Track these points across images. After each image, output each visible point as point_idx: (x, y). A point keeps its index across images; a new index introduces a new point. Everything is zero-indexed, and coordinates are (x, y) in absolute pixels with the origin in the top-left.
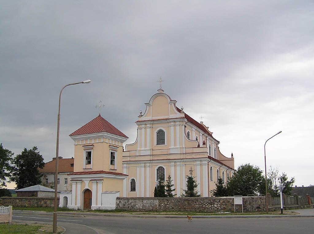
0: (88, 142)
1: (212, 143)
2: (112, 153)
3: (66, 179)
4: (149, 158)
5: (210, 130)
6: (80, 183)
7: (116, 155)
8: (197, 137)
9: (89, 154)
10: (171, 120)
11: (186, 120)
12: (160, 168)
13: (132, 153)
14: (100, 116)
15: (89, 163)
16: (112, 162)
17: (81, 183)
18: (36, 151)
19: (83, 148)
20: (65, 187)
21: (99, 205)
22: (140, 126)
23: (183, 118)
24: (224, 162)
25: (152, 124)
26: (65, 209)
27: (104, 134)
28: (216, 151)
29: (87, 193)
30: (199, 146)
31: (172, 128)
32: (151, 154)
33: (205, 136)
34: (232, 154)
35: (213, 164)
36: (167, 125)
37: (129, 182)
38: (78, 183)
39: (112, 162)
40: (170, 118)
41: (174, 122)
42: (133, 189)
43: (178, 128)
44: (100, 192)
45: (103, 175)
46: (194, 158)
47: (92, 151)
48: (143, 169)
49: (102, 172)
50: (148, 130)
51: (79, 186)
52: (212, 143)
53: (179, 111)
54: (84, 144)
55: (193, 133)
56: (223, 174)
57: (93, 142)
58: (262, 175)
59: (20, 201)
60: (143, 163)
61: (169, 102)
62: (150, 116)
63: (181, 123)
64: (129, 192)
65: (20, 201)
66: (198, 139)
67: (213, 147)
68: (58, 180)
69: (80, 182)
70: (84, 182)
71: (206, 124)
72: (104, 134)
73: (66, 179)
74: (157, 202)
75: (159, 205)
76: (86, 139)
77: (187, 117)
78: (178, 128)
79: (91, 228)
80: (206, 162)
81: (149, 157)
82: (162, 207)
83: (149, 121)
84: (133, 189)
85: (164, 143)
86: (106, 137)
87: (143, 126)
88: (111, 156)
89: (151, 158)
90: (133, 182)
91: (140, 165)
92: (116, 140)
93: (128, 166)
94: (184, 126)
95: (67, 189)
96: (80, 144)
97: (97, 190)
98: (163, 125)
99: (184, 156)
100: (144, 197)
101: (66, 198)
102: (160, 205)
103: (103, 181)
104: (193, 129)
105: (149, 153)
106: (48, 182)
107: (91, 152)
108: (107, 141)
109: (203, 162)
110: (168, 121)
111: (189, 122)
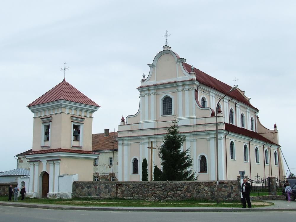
0: (47, 114)
5: (247, 95)
6: (38, 165)
7: (82, 129)
9: (48, 127)
10: (178, 84)
13: (134, 127)
14: (64, 80)
15: (48, 139)
16: (76, 137)
19: (41, 121)
22: (143, 93)
24: (265, 136)
27: (62, 103)
29: (45, 176)
31: (180, 93)
34: (275, 124)
35: (232, 137)
36: (173, 90)
38: (56, 164)
39: (76, 137)
43: (187, 93)
45: (59, 154)
46: (207, 131)
47: (50, 124)
49: (60, 150)
51: (37, 167)
55: (211, 99)
58: (180, 150)
60: (146, 138)
61: (176, 61)
62: (155, 80)
63: (191, 87)
64: (131, 175)
69: (38, 162)
70: (42, 163)
72: (62, 103)
76: (45, 110)
78: (187, 93)
83: (152, 86)
85: (171, 112)
86: (66, 107)
87: (147, 92)
91: (143, 141)
93: (129, 142)
96: (39, 116)
97: (54, 172)
98: (169, 90)
99: (195, 129)
100: (121, 181)
101: (23, 183)
103: (59, 161)
104: (247, 110)
105: (152, 126)
107: (49, 126)
108: (67, 111)
110: (175, 85)
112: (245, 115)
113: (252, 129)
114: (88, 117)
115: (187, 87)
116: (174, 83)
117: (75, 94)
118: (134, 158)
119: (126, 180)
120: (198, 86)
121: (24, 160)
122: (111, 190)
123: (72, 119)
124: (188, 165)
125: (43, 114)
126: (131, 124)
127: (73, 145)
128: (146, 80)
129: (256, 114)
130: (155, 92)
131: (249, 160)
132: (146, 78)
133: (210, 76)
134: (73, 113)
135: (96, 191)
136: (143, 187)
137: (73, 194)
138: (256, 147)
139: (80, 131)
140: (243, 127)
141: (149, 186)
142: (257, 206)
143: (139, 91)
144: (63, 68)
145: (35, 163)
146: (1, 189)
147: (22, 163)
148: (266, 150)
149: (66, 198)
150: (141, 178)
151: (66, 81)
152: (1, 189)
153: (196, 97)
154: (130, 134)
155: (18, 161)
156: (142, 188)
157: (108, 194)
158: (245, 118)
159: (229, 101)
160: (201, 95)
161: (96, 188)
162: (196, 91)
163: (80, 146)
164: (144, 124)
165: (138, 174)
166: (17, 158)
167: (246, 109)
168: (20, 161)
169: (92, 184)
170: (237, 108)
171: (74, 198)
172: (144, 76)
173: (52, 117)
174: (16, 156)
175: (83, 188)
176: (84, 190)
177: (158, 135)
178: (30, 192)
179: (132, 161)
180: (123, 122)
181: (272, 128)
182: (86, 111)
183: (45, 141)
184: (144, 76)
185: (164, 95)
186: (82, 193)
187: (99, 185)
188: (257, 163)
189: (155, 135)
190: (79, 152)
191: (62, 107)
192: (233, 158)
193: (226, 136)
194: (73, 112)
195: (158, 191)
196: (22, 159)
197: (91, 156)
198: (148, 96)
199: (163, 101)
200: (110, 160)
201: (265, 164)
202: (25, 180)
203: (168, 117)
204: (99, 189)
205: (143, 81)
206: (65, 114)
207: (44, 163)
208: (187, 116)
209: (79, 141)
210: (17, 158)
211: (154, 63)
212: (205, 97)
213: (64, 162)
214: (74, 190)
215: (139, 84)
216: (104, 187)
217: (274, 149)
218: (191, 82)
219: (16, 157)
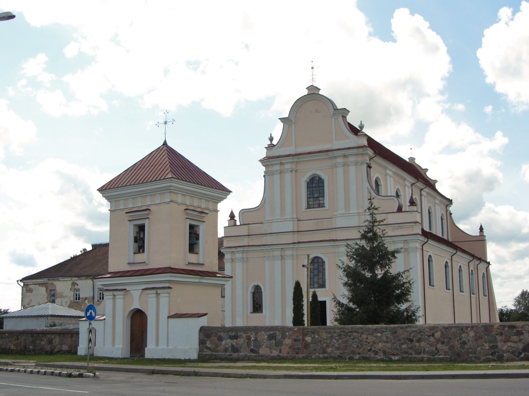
0: (139, 203)
1: (386, 174)
2: (192, 227)
4: (289, 239)
5: (430, 175)
8: (430, 207)
9: (141, 228)
10: (336, 153)
11: (370, 152)
13: (255, 229)
14: (165, 144)
16: (193, 247)
17: (124, 295)
18: (520, 297)
19: (127, 217)
22: (271, 169)
23: (364, 146)
25: (297, 162)
26: (92, 358)
28: (445, 221)
30: (400, 209)
31: (340, 170)
32: (296, 230)
33: (418, 187)
37: (247, 292)
38: (161, 295)
39: (193, 247)
40: (334, 148)
41: (345, 156)
42: (257, 307)
43: (352, 169)
44: (164, 314)
46: (391, 236)
47: (146, 222)
48: (278, 263)
50: (288, 176)
52: (435, 204)
53: (355, 131)
56: (460, 270)
57: (148, 203)
61: (332, 114)
63: (360, 159)
64: (249, 314)
66: (401, 193)
67: (438, 211)
68: (78, 293)
69: (122, 293)
70: (130, 292)
71: (421, 162)
73: (100, 290)
77: (373, 144)
79: (324, 365)
80: (418, 245)
81: (290, 236)
84: (257, 307)
87: (277, 168)
88: (190, 233)
89: (296, 238)
90: (257, 293)
92: (201, 197)
93: (245, 256)
94: (365, 166)
96: (122, 207)
103: (169, 290)
104: (388, 172)
105: (289, 226)
106: (81, 296)
108: (180, 199)
109: (411, 245)
110: (330, 154)
111: (377, 156)
112: (432, 211)
113: (443, 235)
114: (211, 211)
115: (352, 159)
116: (328, 153)
117: (188, 168)
118: (255, 285)
119: (240, 323)
120: (371, 159)
122: (282, 342)
123: (187, 214)
124: (403, 297)
125: (131, 205)
126: (249, 224)
127: (189, 262)
128: (274, 146)
129: (448, 207)
130: (294, 166)
131: (451, 288)
132: (275, 142)
133: (375, 141)
134: (188, 203)
135: (248, 344)
136: (350, 336)
137: (201, 350)
138: (459, 265)
139: (198, 235)
140: (430, 231)
141: (362, 333)
142: (501, 368)
143: (264, 166)
144: (162, 121)
145: (115, 293)
146: (45, 340)
148: (430, 256)
150: (291, 320)
151: (169, 144)
152: (45, 340)
153: (368, 175)
154: (245, 242)
155: (25, 289)
156: (348, 337)
157: (275, 349)
158: (433, 215)
159: (412, 185)
160: (375, 174)
161: (249, 338)
162: (369, 167)
163: (201, 262)
164: (273, 223)
165: (262, 312)
166: (22, 284)
167: (405, 179)
168: (27, 290)
169: (240, 331)
170: (423, 198)
171: (202, 359)
172: (271, 139)
173: (150, 210)
174: (21, 281)
175: (220, 339)
176: (224, 343)
177: (300, 244)
179: (251, 290)
180: (233, 221)
181: (477, 233)
182: (208, 198)
183: (135, 253)
184: (271, 139)
186: (219, 348)
187: (257, 333)
188: (461, 293)
189: (295, 243)
190: (182, 272)
191: (171, 192)
193: (452, 257)
194: (188, 201)
195: (380, 342)
196: (30, 286)
197: (217, 280)
198: (290, 173)
199: (308, 183)
201: (472, 295)
203: (315, 212)
204: (256, 340)
205: (271, 147)
206: (176, 204)
207: (136, 292)
208: (354, 210)
209: (197, 253)
210: (22, 284)
212: (380, 177)
213: (176, 289)
214: (202, 342)
215: (263, 154)
216: (266, 337)
217: (482, 266)
218: (360, 151)
219: (19, 282)
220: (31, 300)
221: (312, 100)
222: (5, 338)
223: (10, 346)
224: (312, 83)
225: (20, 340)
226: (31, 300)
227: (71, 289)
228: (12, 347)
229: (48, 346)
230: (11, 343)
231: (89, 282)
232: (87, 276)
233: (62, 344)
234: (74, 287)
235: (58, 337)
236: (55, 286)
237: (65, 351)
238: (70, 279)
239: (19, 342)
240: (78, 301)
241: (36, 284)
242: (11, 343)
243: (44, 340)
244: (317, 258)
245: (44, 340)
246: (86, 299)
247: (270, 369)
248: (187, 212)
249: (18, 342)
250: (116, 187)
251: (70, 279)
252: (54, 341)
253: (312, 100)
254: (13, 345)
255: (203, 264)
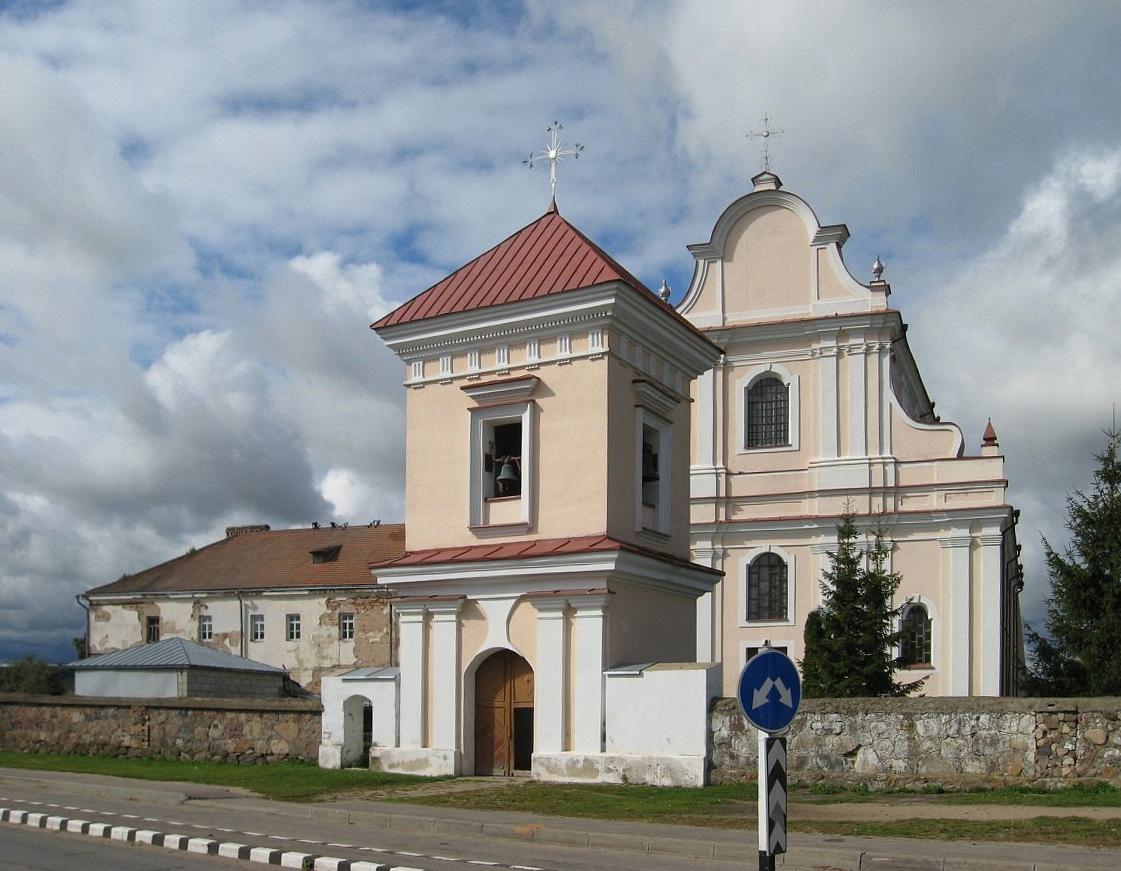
0: (496, 363)
3: (293, 618)
6: (453, 617)
12: (764, 561)
20: (290, 654)
21: (586, 747)
51: (444, 627)
54: (470, 377)
59: (88, 718)
65: (88, 718)
74: (1022, 727)
75: (1043, 751)
76: (483, 345)
78: (854, 364)
82: (1069, 760)
85: (786, 438)
95: (300, 662)
102: (1048, 745)
107: (520, 425)
121: (115, 611)
146: (221, 727)
147: (108, 623)
149: (667, 782)
152: (221, 727)
174: (84, 596)
178: (404, 746)
185: (762, 369)
192: (92, 651)
200: (289, 623)
202: (379, 694)
211: (716, 240)
219: (80, 598)
220: (107, 636)
221: (753, 209)
222: (106, 719)
223: (122, 738)
224: (764, 167)
225: (147, 723)
226: (107, 636)
227: (192, 616)
228: (127, 741)
229: (230, 741)
230: (123, 731)
231: (234, 604)
232: (228, 593)
233: (270, 738)
234: (200, 610)
235: (258, 719)
236: (159, 609)
237: (279, 754)
238: (190, 596)
239: (146, 728)
240: (207, 640)
241: (118, 604)
242: (123, 731)
243: (216, 726)
244: (769, 555)
245: (216, 726)
246: (225, 636)
247: (898, 822)
248: (638, 389)
249: (143, 730)
250: (421, 317)
251: (190, 596)
252: (246, 729)
253: (753, 209)
254: (131, 735)
255: (666, 536)
